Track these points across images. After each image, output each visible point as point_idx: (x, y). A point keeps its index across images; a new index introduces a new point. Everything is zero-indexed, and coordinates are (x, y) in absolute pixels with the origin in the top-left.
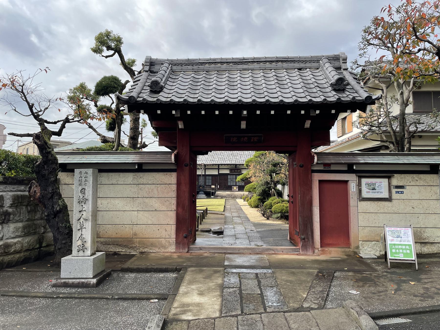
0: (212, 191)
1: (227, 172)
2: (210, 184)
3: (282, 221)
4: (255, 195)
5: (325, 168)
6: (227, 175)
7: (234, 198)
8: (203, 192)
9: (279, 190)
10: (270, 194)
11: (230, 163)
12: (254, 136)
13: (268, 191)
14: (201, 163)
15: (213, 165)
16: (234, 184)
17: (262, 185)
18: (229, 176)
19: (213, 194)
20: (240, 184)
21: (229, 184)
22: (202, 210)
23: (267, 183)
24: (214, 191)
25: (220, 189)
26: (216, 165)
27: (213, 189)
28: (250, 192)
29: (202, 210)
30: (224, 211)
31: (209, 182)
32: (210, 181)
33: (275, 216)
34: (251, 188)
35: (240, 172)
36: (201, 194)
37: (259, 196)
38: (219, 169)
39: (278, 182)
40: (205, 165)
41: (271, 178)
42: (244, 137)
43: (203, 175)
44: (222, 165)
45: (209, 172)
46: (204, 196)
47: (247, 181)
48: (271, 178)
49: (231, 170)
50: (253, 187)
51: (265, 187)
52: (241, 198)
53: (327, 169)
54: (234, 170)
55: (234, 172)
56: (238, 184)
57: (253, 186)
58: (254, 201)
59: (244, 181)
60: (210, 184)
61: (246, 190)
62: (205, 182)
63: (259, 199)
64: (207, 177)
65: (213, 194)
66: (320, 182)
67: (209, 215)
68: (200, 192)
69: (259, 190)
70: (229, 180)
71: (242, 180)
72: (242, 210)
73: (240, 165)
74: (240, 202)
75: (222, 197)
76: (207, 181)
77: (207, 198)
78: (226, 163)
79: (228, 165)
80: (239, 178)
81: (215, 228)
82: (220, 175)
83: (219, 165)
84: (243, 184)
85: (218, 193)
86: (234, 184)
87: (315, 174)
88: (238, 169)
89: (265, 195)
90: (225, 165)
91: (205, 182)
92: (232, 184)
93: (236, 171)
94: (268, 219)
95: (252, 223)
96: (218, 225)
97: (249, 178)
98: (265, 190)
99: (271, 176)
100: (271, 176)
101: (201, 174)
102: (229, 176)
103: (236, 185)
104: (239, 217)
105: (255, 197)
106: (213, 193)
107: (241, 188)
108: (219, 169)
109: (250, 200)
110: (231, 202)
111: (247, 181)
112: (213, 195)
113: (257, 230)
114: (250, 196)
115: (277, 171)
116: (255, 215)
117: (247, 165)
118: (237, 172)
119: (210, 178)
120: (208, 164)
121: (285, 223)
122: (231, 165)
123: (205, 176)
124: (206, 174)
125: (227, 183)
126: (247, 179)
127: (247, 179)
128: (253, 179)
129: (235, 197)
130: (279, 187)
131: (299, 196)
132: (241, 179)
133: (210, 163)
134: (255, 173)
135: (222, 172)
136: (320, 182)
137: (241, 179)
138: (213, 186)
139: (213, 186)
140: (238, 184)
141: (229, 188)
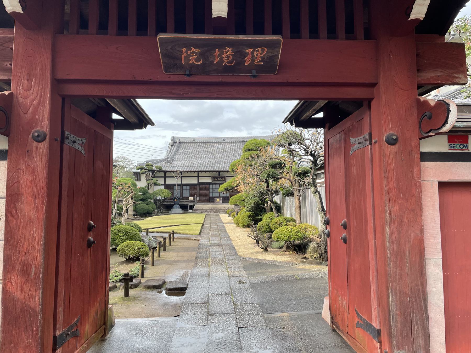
0: (190, 204)
1: (209, 180)
2: (188, 195)
3: (289, 255)
4: (244, 209)
5: (452, 147)
6: (209, 184)
7: (216, 212)
8: (178, 206)
9: (276, 203)
10: (265, 209)
11: (212, 170)
12: (255, 45)
13: (261, 204)
14: (175, 170)
15: (191, 172)
16: (218, 195)
17: (254, 196)
18: (211, 186)
19: (191, 207)
20: (225, 195)
21: (211, 195)
22: (166, 233)
23: (261, 194)
24: (192, 204)
25: (199, 202)
26: (195, 172)
27: (191, 201)
28: (237, 205)
29: (166, 233)
30: (200, 234)
31: (186, 192)
32: (188, 191)
33: (277, 244)
34: (238, 200)
35: (224, 180)
36: (176, 208)
37: (250, 211)
38: (198, 177)
39: (276, 192)
40: (181, 172)
41: (268, 186)
42: (222, 45)
43: (179, 185)
44: (202, 171)
45: (185, 181)
46: (180, 210)
47: (233, 191)
48: (268, 186)
49: (214, 178)
50: (241, 199)
51: (258, 199)
52: (226, 212)
53: (458, 149)
54: (217, 178)
55: (218, 181)
56: (221, 195)
57: (240, 197)
58: (243, 219)
59: (228, 191)
60: (188, 195)
61: (231, 202)
62: (182, 194)
63: (249, 216)
64: (184, 187)
65: (191, 207)
66: (444, 186)
67: (177, 244)
68: (175, 206)
69: (250, 203)
70: (211, 191)
71: (227, 190)
72: (225, 230)
73: (224, 171)
74: (225, 217)
75: (202, 212)
76: (184, 191)
77: (184, 213)
78: (207, 170)
79: (209, 171)
80: (223, 187)
81: (173, 277)
82: (200, 184)
83: (198, 172)
84: (228, 195)
85: (197, 206)
86: (218, 195)
87: (429, 166)
88: (222, 177)
89: (258, 210)
90: (206, 171)
91: (182, 194)
92: (214, 196)
93: (220, 179)
94: (266, 250)
95: (242, 259)
96: (183, 265)
97: (237, 186)
98: (258, 202)
99: (267, 182)
100: (267, 182)
101: (176, 183)
102: (211, 186)
103: (219, 197)
104: (220, 245)
105: (244, 213)
106: (191, 206)
107: (225, 200)
108: (198, 177)
109: (236, 217)
110: (213, 217)
111: (233, 191)
112: (191, 209)
113: (252, 279)
114: (237, 209)
115: (277, 175)
116: (242, 239)
117: (233, 171)
118: (221, 181)
119: (188, 187)
120: (185, 170)
121: (297, 259)
122: (213, 171)
123: (181, 185)
124: (183, 183)
125: (209, 194)
126: (233, 188)
127: (233, 188)
128: (242, 187)
129: (218, 211)
130: (277, 199)
131: (388, 229)
132: (225, 189)
133: (188, 170)
134: (244, 178)
135: (202, 180)
136: (443, 185)
137: (225, 189)
138: (191, 198)
139: (191, 198)
140: (221, 195)
141: (211, 200)
